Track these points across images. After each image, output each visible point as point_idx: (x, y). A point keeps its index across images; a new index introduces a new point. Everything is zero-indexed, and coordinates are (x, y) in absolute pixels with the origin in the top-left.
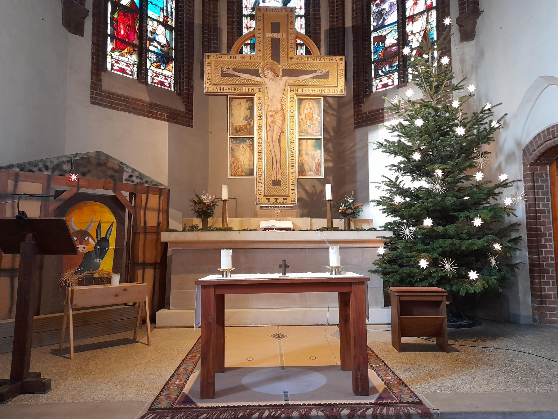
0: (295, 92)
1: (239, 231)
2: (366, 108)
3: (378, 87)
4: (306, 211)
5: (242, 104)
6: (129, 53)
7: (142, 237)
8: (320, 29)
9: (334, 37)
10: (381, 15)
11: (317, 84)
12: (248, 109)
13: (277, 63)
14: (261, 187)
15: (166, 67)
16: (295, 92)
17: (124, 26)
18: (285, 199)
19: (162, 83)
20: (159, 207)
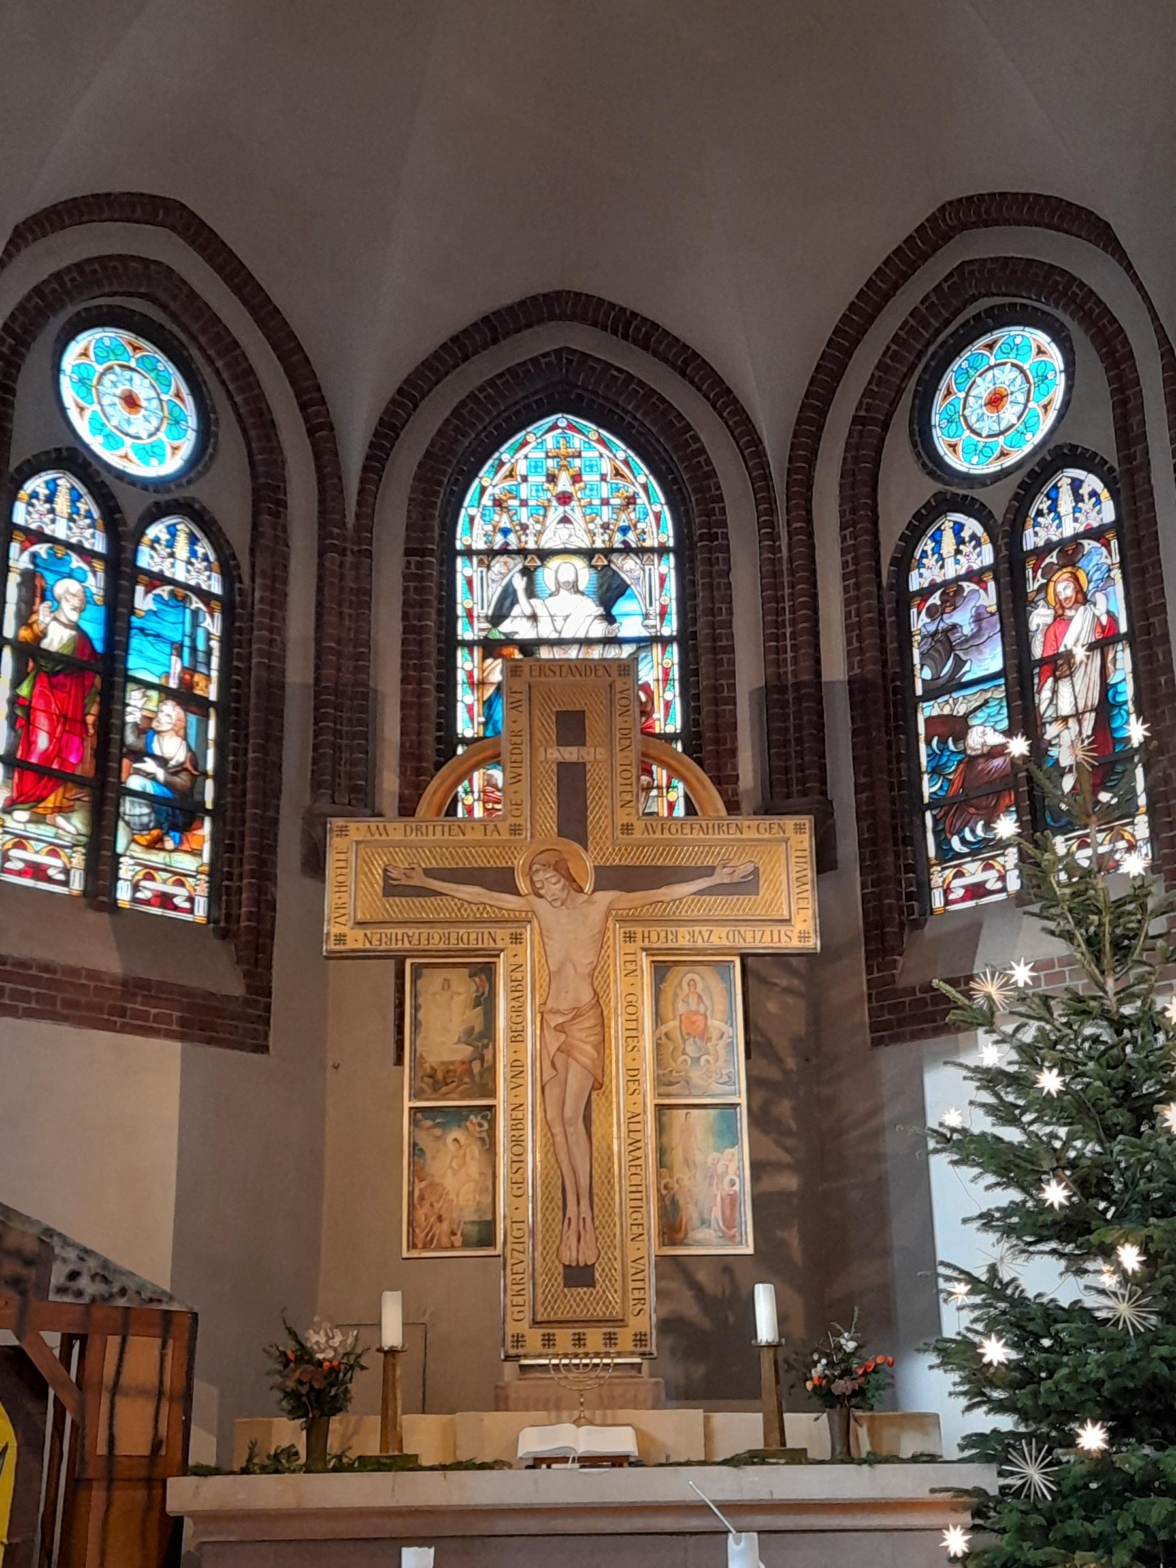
0: (640, 943)
1: (444, 1468)
2: (910, 970)
3: (951, 897)
4: (700, 1370)
5: (455, 986)
6: (60, 810)
7: (98, 1495)
8: (732, 687)
9: (784, 717)
10: (946, 644)
11: (717, 914)
12: (475, 1006)
13: (576, 846)
14: (519, 1295)
15: (181, 842)
16: (640, 943)
17: (51, 720)
18: (610, 1339)
19: (165, 900)
20: (161, 1382)
